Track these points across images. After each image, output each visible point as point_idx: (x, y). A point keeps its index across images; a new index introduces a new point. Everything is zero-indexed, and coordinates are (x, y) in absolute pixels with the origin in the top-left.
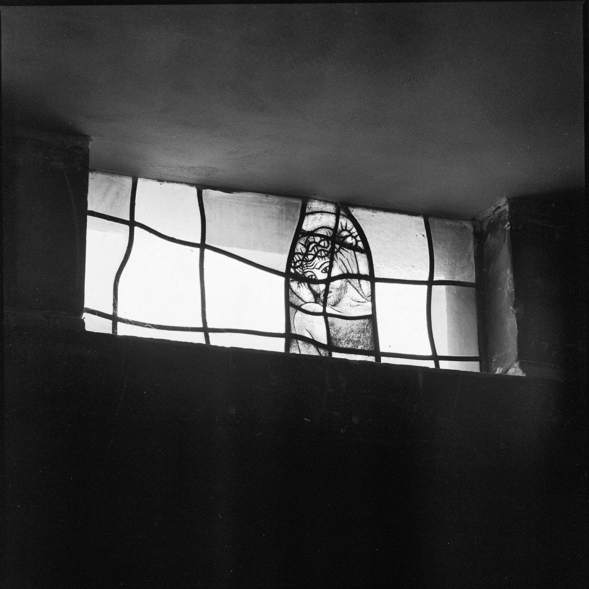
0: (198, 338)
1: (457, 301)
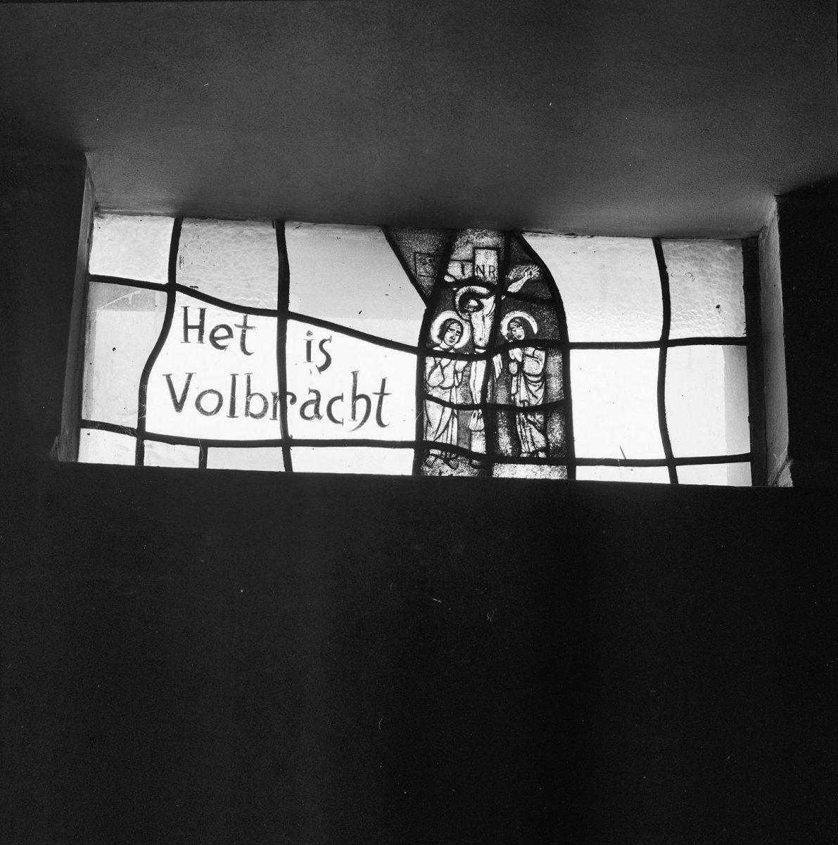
0: (660, 476)
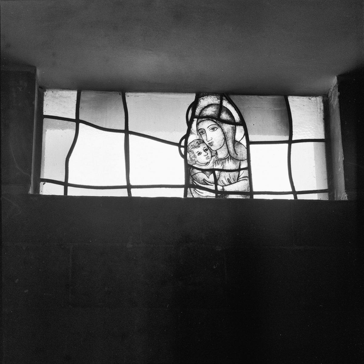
0: (291, 197)
1: (99, 106)
